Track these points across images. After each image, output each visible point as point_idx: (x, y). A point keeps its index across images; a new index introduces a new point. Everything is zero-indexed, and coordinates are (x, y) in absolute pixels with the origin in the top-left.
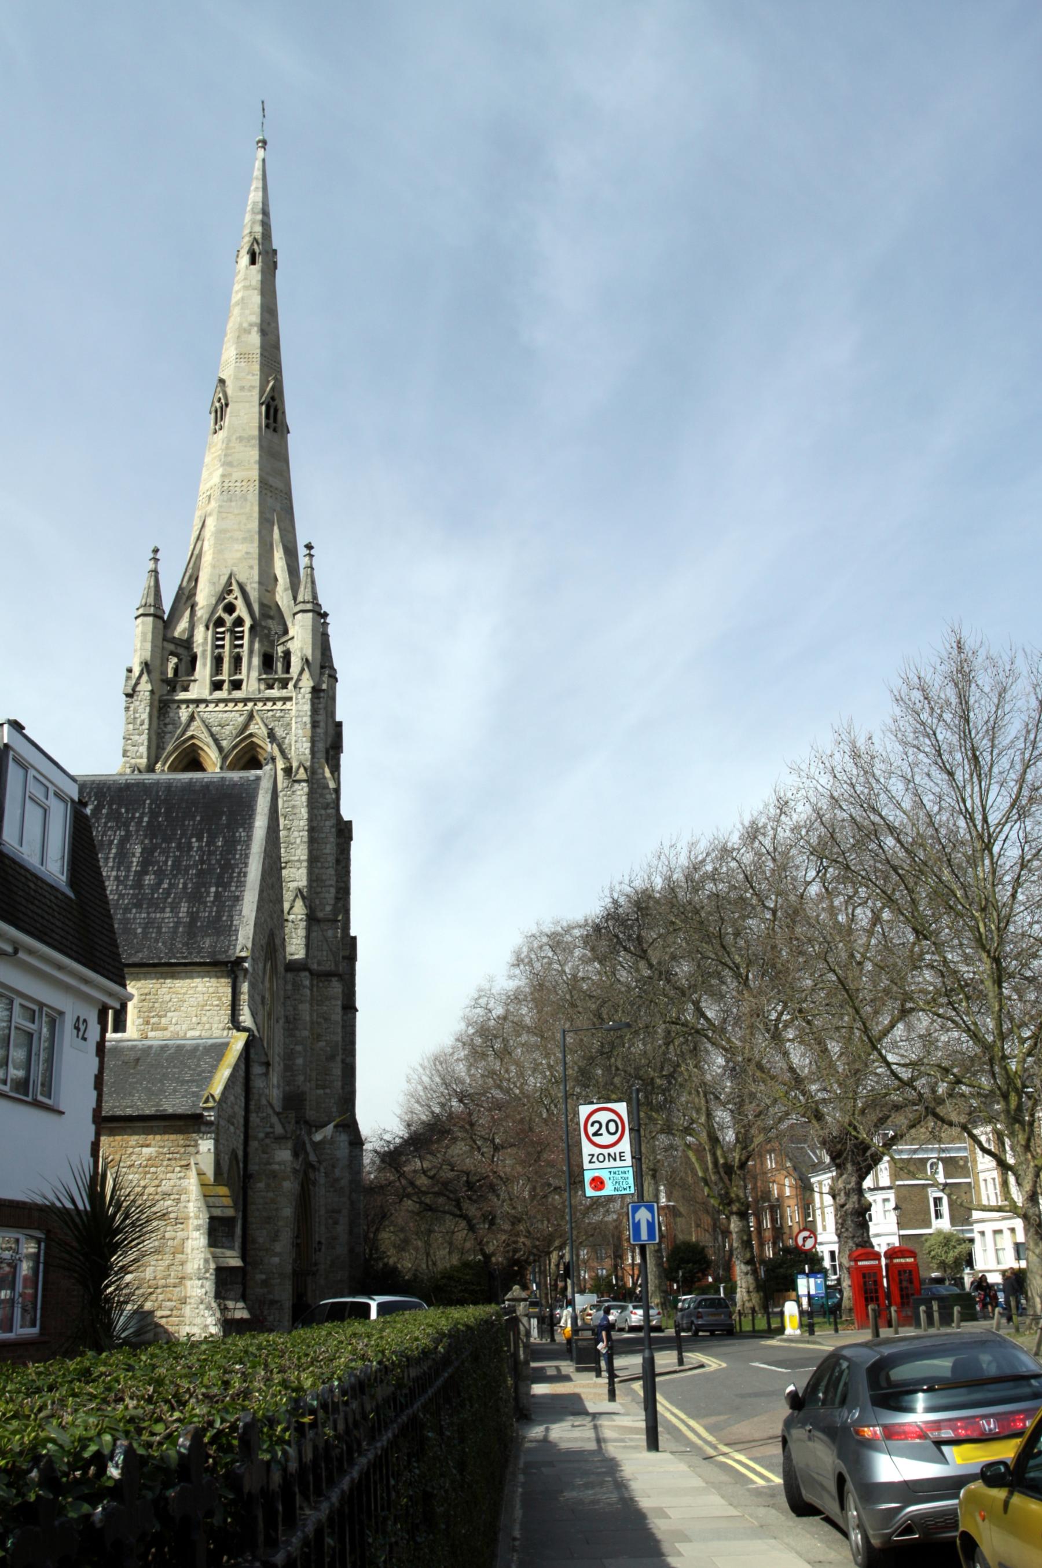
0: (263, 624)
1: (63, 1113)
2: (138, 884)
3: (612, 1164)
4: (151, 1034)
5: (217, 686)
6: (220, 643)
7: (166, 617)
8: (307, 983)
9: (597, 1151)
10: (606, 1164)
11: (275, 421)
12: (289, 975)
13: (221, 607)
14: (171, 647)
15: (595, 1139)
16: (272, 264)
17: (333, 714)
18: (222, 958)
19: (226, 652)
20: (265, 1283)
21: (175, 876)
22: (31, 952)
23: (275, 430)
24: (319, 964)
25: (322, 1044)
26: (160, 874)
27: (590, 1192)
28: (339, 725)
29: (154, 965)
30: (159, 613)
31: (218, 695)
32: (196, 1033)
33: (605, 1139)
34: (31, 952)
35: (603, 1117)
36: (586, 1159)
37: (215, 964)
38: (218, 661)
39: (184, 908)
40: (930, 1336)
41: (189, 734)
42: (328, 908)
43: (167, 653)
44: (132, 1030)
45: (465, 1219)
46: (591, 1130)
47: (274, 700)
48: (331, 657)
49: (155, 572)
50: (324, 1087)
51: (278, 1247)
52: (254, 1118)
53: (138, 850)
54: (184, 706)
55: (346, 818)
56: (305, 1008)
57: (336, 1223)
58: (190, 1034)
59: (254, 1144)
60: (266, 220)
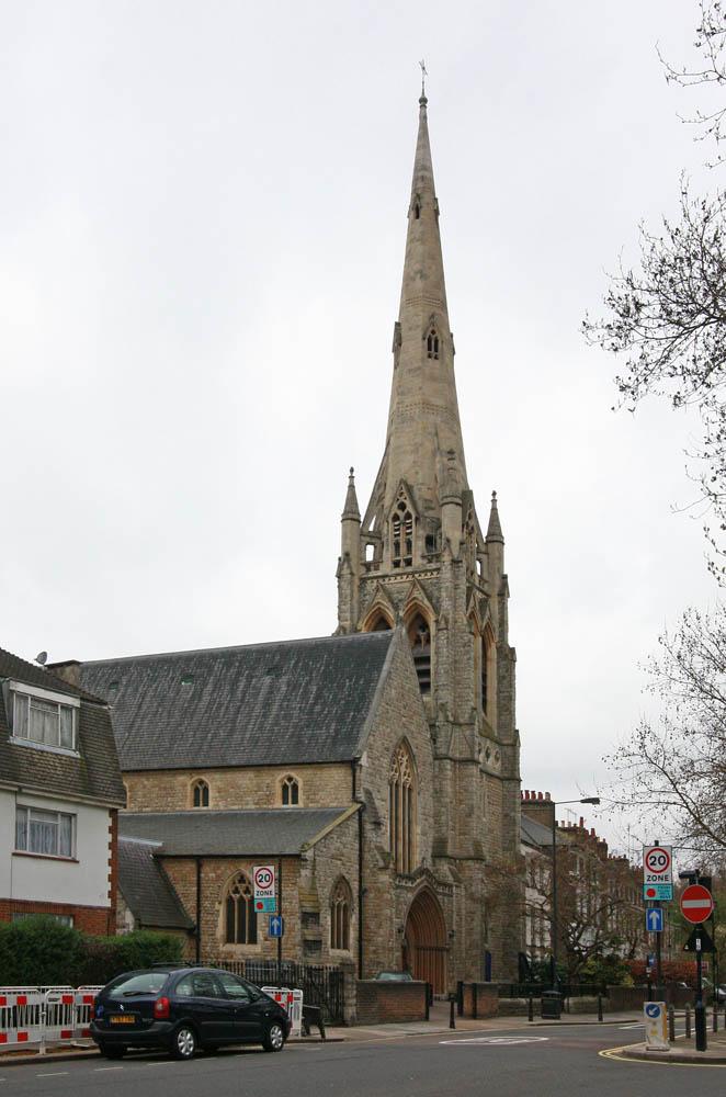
0: (426, 514)
1: (78, 862)
2: (311, 712)
3: (661, 882)
4: (310, 805)
5: (397, 564)
6: (408, 531)
8: (449, 767)
9: (652, 874)
10: (657, 882)
11: (436, 351)
12: (437, 762)
13: (396, 506)
14: (368, 539)
15: (652, 867)
16: (433, 213)
17: (500, 568)
18: (346, 758)
19: (402, 539)
20: (374, 952)
21: (332, 706)
22: (25, 787)
23: (436, 358)
24: (461, 753)
26: (324, 704)
27: (647, 897)
28: (505, 577)
30: (355, 516)
31: (397, 570)
32: (335, 805)
33: (264, 884)
34: (25, 787)
35: (264, 872)
36: (646, 878)
37: (342, 762)
38: (397, 545)
39: (333, 726)
40: (419, 884)
41: (376, 601)
42: (467, 716)
44: (301, 804)
46: (650, 862)
47: (431, 571)
48: (499, 526)
49: (352, 487)
50: (465, 834)
51: (381, 932)
52: (367, 856)
53: (315, 689)
54: (369, 582)
57: (472, 920)
58: (331, 805)
59: (367, 872)
60: (426, 174)
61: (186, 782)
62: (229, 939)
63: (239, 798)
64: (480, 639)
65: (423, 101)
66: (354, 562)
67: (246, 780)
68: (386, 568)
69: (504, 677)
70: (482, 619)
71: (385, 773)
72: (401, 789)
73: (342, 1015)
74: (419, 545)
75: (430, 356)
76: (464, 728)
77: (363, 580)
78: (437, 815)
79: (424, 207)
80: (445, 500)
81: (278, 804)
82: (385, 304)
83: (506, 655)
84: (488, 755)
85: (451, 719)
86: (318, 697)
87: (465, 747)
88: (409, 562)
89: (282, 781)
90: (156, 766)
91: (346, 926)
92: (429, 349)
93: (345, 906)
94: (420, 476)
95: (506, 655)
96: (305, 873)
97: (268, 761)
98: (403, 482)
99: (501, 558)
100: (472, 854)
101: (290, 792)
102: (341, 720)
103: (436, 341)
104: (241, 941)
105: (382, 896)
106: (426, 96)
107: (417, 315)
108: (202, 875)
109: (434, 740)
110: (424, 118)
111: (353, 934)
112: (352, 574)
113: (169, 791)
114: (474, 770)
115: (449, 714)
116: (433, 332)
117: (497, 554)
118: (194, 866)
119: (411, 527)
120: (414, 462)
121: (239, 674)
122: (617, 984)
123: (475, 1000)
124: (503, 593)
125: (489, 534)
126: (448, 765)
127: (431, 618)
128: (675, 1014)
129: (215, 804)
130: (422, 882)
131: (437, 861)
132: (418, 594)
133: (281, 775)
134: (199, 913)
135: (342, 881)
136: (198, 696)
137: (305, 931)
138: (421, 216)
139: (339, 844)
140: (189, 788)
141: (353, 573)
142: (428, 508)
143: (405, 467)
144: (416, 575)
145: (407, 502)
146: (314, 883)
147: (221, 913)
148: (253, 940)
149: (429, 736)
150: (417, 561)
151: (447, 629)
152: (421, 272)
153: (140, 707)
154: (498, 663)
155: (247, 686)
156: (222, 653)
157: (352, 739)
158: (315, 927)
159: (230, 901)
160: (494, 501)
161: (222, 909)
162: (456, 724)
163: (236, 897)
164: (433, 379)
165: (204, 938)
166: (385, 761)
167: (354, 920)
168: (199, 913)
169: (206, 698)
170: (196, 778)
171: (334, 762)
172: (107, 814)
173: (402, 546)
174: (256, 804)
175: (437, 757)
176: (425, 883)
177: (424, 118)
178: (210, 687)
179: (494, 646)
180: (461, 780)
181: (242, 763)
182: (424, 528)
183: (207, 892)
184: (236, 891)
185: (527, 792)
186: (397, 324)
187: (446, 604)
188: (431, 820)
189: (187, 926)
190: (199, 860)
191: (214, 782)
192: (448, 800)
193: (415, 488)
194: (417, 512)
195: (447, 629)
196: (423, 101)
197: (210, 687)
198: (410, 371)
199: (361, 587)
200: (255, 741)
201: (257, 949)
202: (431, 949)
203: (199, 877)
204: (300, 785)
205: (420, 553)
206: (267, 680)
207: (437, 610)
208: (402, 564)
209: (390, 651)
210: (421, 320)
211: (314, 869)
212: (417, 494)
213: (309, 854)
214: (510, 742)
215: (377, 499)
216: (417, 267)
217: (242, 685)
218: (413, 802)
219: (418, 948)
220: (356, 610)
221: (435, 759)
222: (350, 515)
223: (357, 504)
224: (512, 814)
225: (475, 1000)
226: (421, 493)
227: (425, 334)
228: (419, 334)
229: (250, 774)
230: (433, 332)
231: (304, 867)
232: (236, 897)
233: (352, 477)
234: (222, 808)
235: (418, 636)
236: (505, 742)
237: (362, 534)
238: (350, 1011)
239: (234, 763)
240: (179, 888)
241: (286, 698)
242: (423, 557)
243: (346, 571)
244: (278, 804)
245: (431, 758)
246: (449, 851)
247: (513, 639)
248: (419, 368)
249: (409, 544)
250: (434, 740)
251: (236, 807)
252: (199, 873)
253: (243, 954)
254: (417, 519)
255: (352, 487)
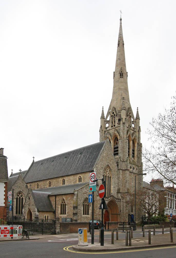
4: (84, 182)
5: (112, 127)
7: (105, 118)
8: (121, 171)
9: (91, 182)
11: (122, 76)
12: (118, 171)
13: (112, 113)
14: (106, 122)
16: (122, 45)
19: (113, 121)
23: (122, 78)
25: (125, 181)
29: (84, 172)
30: (103, 117)
31: (112, 128)
38: (112, 122)
40: (110, 199)
42: (126, 159)
43: (105, 123)
44: (82, 182)
45: (141, 203)
49: (103, 111)
50: (125, 187)
51: (97, 211)
55: (141, 143)
56: (121, 177)
60: (121, 36)
61: (61, 179)
62: (61, 214)
63: (70, 182)
64: (132, 141)
65: (121, 20)
66: (103, 128)
67: (72, 178)
68: (110, 128)
69: (139, 150)
70: (132, 137)
71: (101, 173)
72: (107, 177)
73: (55, 231)
74: (117, 121)
75: (121, 78)
76: (125, 162)
77: (105, 132)
78: (118, 183)
79: (121, 44)
80: (122, 109)
81: (78, 183)
82: (112, 67)
83: (140, 145)
84: (134, 169)
85: (122, 160)
86: (89, 157)
87: (125, 167)
88: (114, 126)
89: (78, 177)
90: (56, 177)
91: (88, 210)
92: (121, 76)
93: (88, 205)
94: (117, 105)
95: (140, 145)
96: (75, 197)
97: (76, 173)
98: (113, 107)
99: (139, 123)
100: (127, 192)
101: (80, 179)
102: (92, 162)
103: (122, 74)
104: (63, 214)
105: (98, 202)
106: (122, 18)
107: (118, 69)
108: (56, 199)
109: (118, 165)
110: (121, 23)
111: (90, 211)
112: (102, 130)
113: (58, 182)
114: (127, 172)
115: (122, 159)
116: (122, 72)
117: (138, 122)
118: (55, 197)
119: (115, 118)
120: (116, 102)
121: (75, 155)
122: (165, 221)
123: (108, 227)
124: (139, 131)
125: (136, 117)
126: (121, 171)
127: (118, 137)
128: (155, 230)
129: (66, 184)
130: (111, 199)
131: (118, 194)
132: (116, 132)
133: (78, 176)
134: (55, 208)
135: (86, 199)
136: (67, 161)
137: (74, 211)
138: (119, 46)
139: (86, 190)
140: (62, 181)
141: (103, 130)
142: (119, 112)
143: (114, 105)
144: (116, 128)
145: (114, 112)
146: (77, 199)
147: (59, 207)
148: (65, 214)
149: (116, 165)
150: (116, 125)
151: (121, 139)
152: (119, 59)
153: (56, 165)
154: (138, 147)
155: (76, 157)
156: (73, 151)
157: (93, 166)
158: (77, 210)
159: (61, 205)
160: (137, 110)
161: (60, 207)
162: (123, 161)
163: (62, 204)
164: (121, 82)
165: (56, 214)
166: (102, 171)
167: (91, 208)
168: (55, 208)
169: (68, 161)
170: (63, 179)
171: (88, 172)
172: (4, 183)
173: (113, 122)
174: (74, 183)
175: (118, 170)
176: (112, 199)
177: (121, 23)
178: (69, 159)
179: (136, 143)
180: (124, 174)
181: (71, 174)
182: (118, 117)
183: (57, 203)
184: (62, 203)
185: (156, 179)
186: (114, 72)
187: (121, 134)
188: (117, 184)
189: (53, 211)
190: (56, 196)
191: (66, 179)
192: (121, 179)
193: (116, 109)
194: (116, 114)
195: (121, 139)
196: (121, 20)
197: (69, 159)
198: (116, 82)
199: (104, 133)
200: (74, 169)
201: (66, 215)
202: (115, 214)
203: (56, 200)
204: (82, 178)
205: (117, 123)
206: (80, 155)
207: (119, 135)
208: (113, 126)
209: (104, 145)
210: (119, 69)
211: (77, 196)
212: (117, 109)
213: (76, 193)
214: (140, 165)
215: (108, 113)
216: (118, 58)
217: (75, 157)
218: (111, 180)
219: (112, 214)
220: (103, 139)
221: (118, 170)
222: (102, 117)
223: (104, 114)
224: (140, 182)
225: (108, 227)
226: (118, 109)
227: (119, 73)
228: (118, 73)
229: (73, 176)
230: (122, 72)
231: (75, 196)
232: (62, 204)
233: (103, 109)
234: (67, 185)
235: (117, 142)
236: (139, 165)
237: (105, 121)
238: (58, 230)
239: (69, 174)
240: (52, 203)
241: (82, 159)
242: (118, 124)
243: (101, 130)
244: (78, 183)
245: (117, 170)
246: (121, 191)
247: (141, 141)
248: (118, 81)
249: (115, 121)
250: (118, 165)
251: (70, 184)
252: (56, 199)
253: (63, 217)
254: (116, 115)
255: (103, 111)
